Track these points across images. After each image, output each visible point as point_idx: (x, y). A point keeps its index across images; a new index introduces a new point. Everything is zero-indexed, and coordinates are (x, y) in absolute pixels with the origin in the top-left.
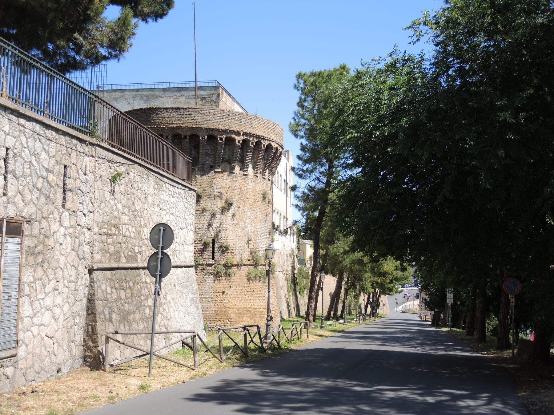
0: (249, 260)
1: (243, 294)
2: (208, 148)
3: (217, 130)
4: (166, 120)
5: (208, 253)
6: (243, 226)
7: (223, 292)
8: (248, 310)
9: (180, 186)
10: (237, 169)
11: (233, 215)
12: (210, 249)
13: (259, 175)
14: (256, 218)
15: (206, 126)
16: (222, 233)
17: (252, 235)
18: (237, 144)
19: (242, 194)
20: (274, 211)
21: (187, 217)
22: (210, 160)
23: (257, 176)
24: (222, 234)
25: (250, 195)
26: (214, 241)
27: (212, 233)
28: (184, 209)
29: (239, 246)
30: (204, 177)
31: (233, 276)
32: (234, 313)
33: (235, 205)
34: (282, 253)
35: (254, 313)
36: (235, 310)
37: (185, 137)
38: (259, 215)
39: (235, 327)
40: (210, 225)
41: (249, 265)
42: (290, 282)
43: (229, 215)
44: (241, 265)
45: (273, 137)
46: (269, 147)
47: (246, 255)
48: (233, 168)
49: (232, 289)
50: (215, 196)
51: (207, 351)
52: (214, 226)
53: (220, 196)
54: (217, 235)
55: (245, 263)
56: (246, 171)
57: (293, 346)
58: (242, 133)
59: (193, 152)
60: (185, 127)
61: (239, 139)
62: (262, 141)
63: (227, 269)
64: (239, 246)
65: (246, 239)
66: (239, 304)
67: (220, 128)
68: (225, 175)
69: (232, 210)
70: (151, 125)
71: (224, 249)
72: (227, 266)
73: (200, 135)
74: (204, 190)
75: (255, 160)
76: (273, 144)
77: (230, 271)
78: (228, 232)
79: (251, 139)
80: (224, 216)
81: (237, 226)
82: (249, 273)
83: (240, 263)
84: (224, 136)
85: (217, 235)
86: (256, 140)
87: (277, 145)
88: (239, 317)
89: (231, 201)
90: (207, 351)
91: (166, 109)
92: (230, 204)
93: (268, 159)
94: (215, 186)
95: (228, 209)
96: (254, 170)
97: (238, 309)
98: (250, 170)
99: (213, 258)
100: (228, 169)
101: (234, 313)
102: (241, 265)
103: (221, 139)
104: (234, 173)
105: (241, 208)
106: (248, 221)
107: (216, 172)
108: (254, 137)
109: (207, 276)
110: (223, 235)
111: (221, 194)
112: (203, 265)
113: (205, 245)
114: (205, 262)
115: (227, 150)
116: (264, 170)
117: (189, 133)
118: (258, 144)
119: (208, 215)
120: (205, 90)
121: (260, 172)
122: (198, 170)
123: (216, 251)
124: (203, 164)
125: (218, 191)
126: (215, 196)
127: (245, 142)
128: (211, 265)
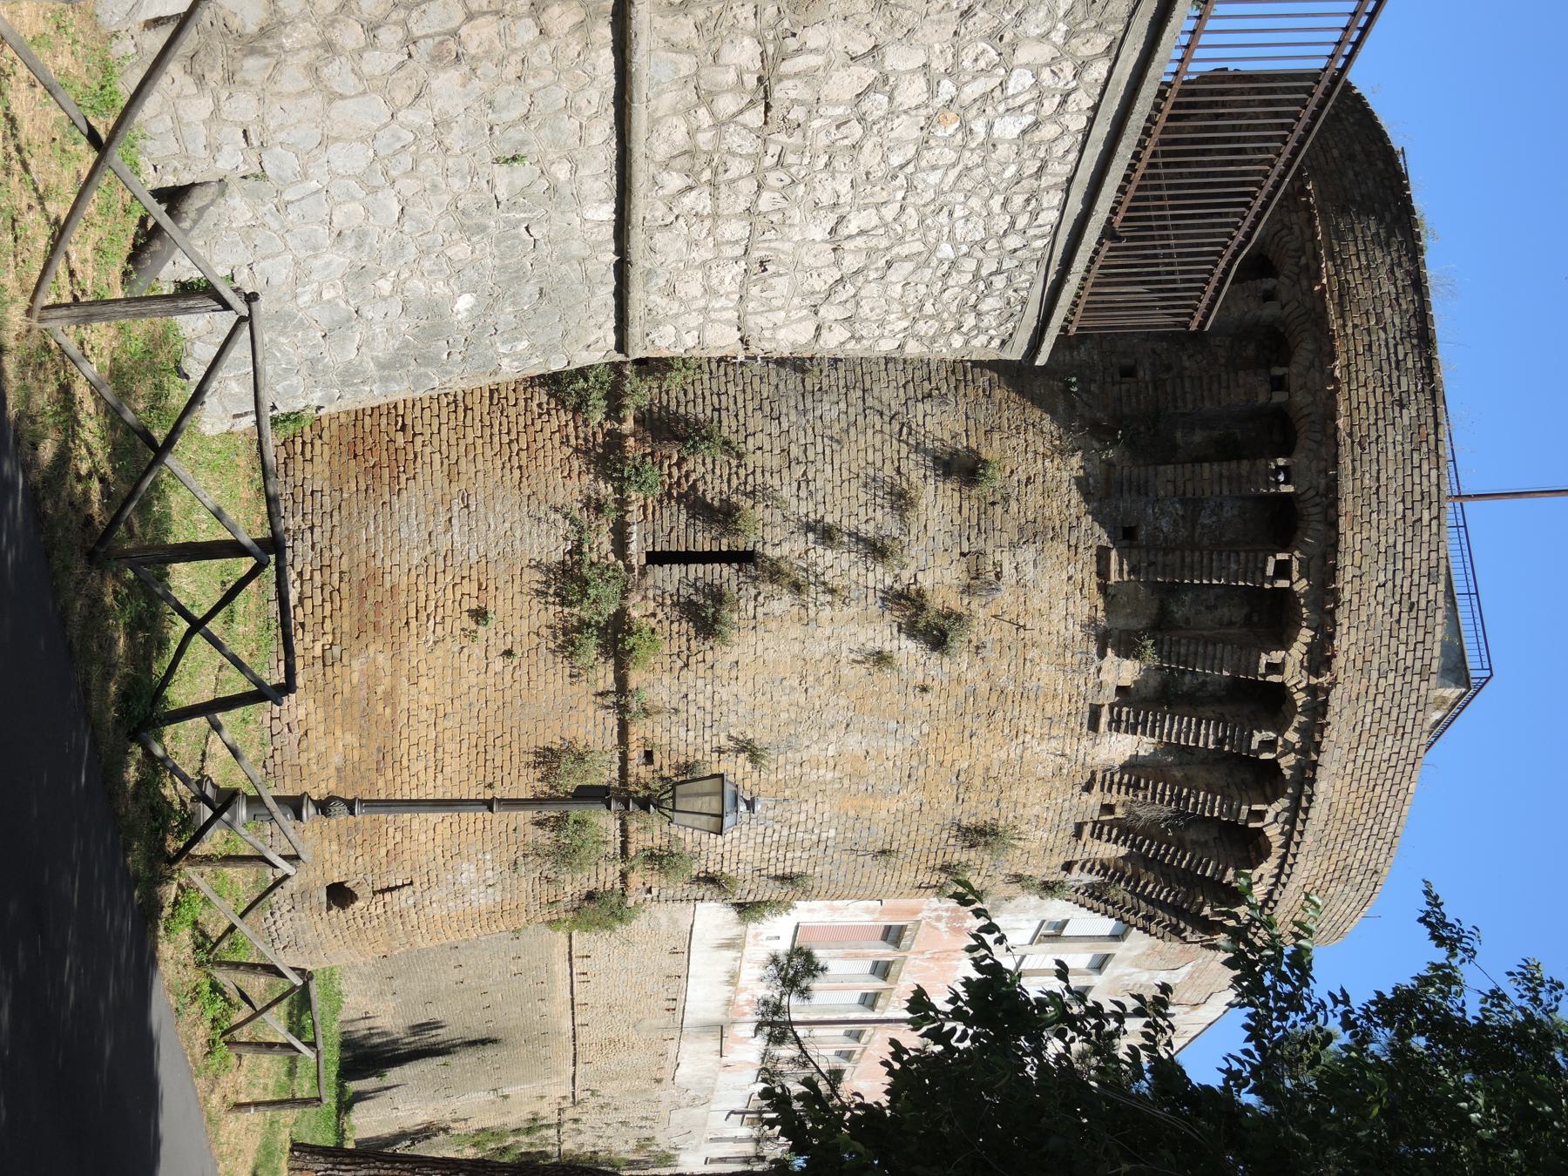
0: (649, 756)
1: (472, 726)
2: (1228, 513)
3: (1331, 546)
4: (1358, 278)
5: (679, 530)
6: (829, 716)
7: (480, 615)
9: (1075, 206)
10: (1125, 671)
11: (881, 659)
12: (704, 543)
13: (1095, 799)
14: (871, 791)
15: (1346, 485)
16: (787, 598)
18: (1264, 659)
19: (995, 705)
20: (857, 1036)
21: (896, 275)
22: (1165, 524)
23: (1088, 788)
24: (783, 603)
25: (992, 751)
26: (744, 558)
27: (786, 548)
28: (946, 251)
29: (724, 693)
30: (1076, 496)
32: (371, 680)
33: (935, 667)
34: (658, 1091)
36: (387, 681)
37: (1279, 384)
38: (885, 809)
40: (826, 534)
41: (624, 759)
42: (525, 1144)
43: (883, 634)
44: (622, 709)
45: (1305, 869)
46: (1251, 847)
48: (1128, 648)
49: (498, 664)
50: (980, 554)
51: (93, 136)
52: (825, 558)
53: (979, 581)
54: (775, 573)
55: (636, 731)
56: (1115, 725)
57: (174, 952)
58: (1324, 680)
59: (1198, 437)
60: (1335, 381)
61: (1289, 664)
62: (1284, 802)
63: (602, 631)
64: (724, 693)
65: (760, 735)
66: (420, 697)
67: (1345, 560)
68: (1089, 605)
69: (909, 650)
70: (1326, 220)
71: (704, 617)
72: (616, 638)
73: (1299, 458)
74: (1006, 499)
75: (1178, 774)
76: (1268, 867)
77: (591, 647)
78: (796, 631)
79: (1292, 736)
80: (875, 609)
81: (828, 681)
82: (580, 758)
83: (634, 706)
84: (1301, 586)
85: (775, 573)
86: (1287, 762)
87: (1259, 893)
88: (348, 704)
89: (956, 643)
90: (93, 136)
91: (1418, 284)
92: (937, 638)
93: (1181, 846)
94: (1028, 553)
95: (911, 630)
96: (1124, 768)
97: (390, 697)
98: (1120, 747)
99: (655, 558)
100: (1121, 623)
101: (371, 680)
102: (622, 709)
103: (1283, 570)
104: (1102, 655)
105: (918, 703)
106: (853, 743)
107: (1102, 555)
108: (1304, 751)
109: (564, 526)
110: (776, 607)
111: (992, 588)
112: (622, 503)
113: (724, 515)
114: (634, 514)
115: (1224, 612)
116: (1124, 830)
117: (1300, 398)
118: (1266, 780)
119: (880, 522)
121: (1108, 808)
122: (1109, 464)
123: (696, 570)
124: (1142, 489)
125: (1008, 569)
126: (980, 554)
127: (1270, 702)
128: (620, 546)
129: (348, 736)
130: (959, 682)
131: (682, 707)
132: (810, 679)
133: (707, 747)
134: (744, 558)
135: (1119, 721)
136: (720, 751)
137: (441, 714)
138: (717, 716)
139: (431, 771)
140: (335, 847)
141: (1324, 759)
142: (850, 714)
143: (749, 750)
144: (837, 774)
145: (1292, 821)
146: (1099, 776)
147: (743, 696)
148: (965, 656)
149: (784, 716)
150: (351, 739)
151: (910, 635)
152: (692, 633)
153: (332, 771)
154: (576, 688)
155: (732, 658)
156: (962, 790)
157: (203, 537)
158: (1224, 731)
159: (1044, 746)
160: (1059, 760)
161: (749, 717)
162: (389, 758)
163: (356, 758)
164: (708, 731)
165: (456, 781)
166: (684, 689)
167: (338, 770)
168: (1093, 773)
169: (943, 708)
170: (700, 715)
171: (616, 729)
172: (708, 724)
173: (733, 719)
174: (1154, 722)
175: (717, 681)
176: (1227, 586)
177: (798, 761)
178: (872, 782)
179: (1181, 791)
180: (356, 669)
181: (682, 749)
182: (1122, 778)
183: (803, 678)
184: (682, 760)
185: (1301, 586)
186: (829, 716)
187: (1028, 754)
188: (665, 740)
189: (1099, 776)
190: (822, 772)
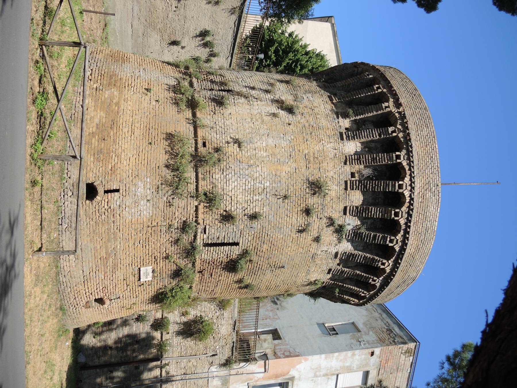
0: (204, 145)
6: (262, 131)
8: (114, 123)
10: (346, 123)
11: (274, 115)
17: (247, 151)
26: (228, 91)
29: (228, 122)
31: (174, 108)
35: (108, 135)
39: (87, 93)
40: (253, 88)
41: (196, 143)
43: (274, 109)
47: (214, 138)
48: (345, 116)
52: (253, 92)
64: (228, 122)
69: (282, 113)
71: (219, 102)
78: (247, 107)
79: (399, 127)
81: (259, 120)
95: (282, 108)
96: (355, 154)
97: (118, 104)
98: (352, 147)
104: (338, 118)
120: (402, 331)
129: (102, 113)
130: (299, 123)
131: (214, 126)
132: (254, 119)
133: (224, 141)
134: (228, 91)
135: (349, 137)
136: (228, 143)
137: (134, 113)
138: (226, 130)
139: (130, 132)
140: (92, 159)
141: (410, 131)
142: (268, 131)
143: (238, 142)
144: (267, 154)
145: (409, 159)
146: (348, 158)
147: (234, 124)
148: (299, 116)
149: (247, 130)
150: (103, 114)
151: (282, 110)
152: (216, 105)
153: (95, 124)
154: (179, 115)
155: (229, 112)
156: (307, 163)
157: (58, 93)
158: (380, 131)
159: (329, 146)
160: (335, 151)
161: (236, 131)
162: (115, 124)
163: (104, 121)
164: (223, 135)
165: (138, 139)
166: (215, 120)
167: (97, 125)
168: (346, 156)
169: (296, 130)
170: (220, 129)
171: (193, 132)
172: (223, 132)
173: (231, 131)
174: (359, 134)
175: (225, 119)
176: (366, 96)
177: (254, 148)
178: (279, 158)
179: (373, 156)
180: (107, 94)
181: (215, 141)
182: (355, 157)
183: (252, 119)
184: (216, 146)
185: (385, 90)
186: (262, 131)
187: (325, 148)
188: (210, 138)
189: (348, 158)
190: (262, 152)
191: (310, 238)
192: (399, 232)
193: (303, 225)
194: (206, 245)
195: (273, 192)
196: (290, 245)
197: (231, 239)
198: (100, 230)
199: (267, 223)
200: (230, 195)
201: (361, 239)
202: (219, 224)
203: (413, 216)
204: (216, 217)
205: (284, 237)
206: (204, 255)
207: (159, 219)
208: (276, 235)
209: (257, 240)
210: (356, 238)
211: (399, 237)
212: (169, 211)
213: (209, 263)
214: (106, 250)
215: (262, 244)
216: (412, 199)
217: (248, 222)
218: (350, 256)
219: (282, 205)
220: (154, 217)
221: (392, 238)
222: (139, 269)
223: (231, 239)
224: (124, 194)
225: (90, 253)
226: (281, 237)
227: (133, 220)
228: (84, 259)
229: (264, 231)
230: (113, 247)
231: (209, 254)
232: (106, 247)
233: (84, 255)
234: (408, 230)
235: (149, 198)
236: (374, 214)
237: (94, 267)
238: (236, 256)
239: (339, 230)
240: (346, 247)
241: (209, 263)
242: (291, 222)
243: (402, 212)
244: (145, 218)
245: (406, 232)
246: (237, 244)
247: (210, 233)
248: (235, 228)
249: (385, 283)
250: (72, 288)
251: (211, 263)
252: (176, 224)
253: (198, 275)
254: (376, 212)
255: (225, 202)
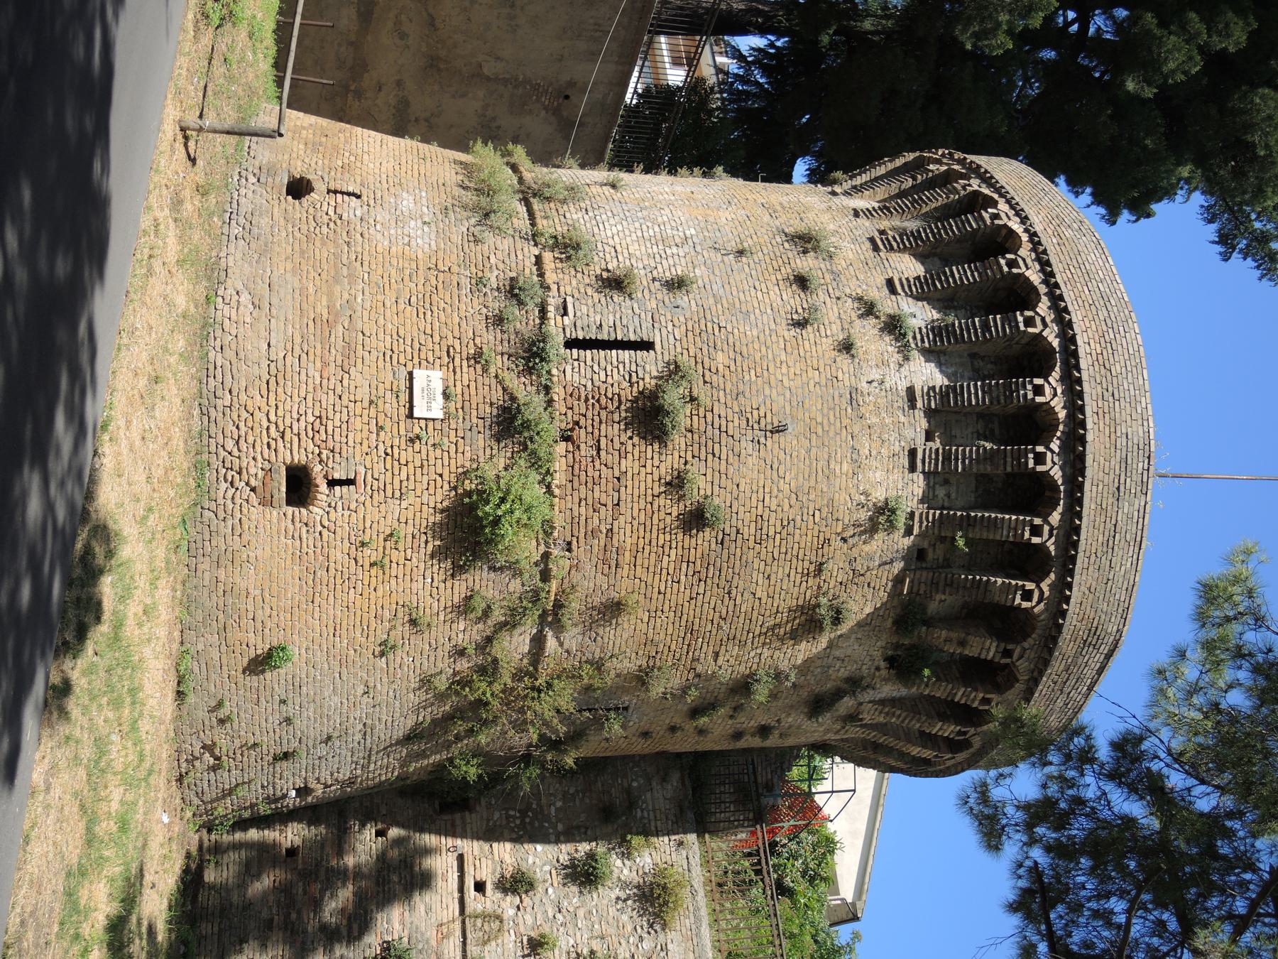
191: (827, 344)
192: (1052, 369)
193: (800, 311)
194: (571, 344)
195: (710, 243)
196: (783, 358)
197: (631, 330)
198: (317, 251)
199: (711, 301)
200: (611, 242)
201: (956, 339)
202: (596, 295)
203: (1053, 261)
204: (587, 281)
205: (762, 336)
206: (572, 372)
207: (452, 260)
208: (742, 330)
209: (697, 339)
210: (938, 347)
211: (1043, 307)
212: (476, 251)
213: (587, 400)
214: (329, 300)
215: (712, 350)
216: (1033, 235)
217: (663, 294)
218: (948, 395)
219: (735, 267)
220: (441, 254)
221: (1028, 313)
222: (411, 374)
223: (631, 330)
224: (372, 202)
225: (289, 297)
226: (755, 333)
227: (394, 249)
228: (274, 311)
229: (709, 317)
230: (346, 296)
231: (583, 371)
232: (330, 295)
233: (275, 301)
234: (1063, 304)
235: (426, 219)
236: (961, 278)
237: (298, 340)
238: (653, 382)
239: (893, 326)
240: (926, 374)
241: (587, 400)
242: (767, 300)
243: (1024, 260)
244: (420, 252)
245: (1053, 287)
246: (647, 346)
247: (578, 314)
248: (635, 306)
249: (1073, 466)
250: (235, 393)
251: (595, 399)
252: (493, 279)
253: (561, 447)
254: (963, 274)
255: (601, 254)
